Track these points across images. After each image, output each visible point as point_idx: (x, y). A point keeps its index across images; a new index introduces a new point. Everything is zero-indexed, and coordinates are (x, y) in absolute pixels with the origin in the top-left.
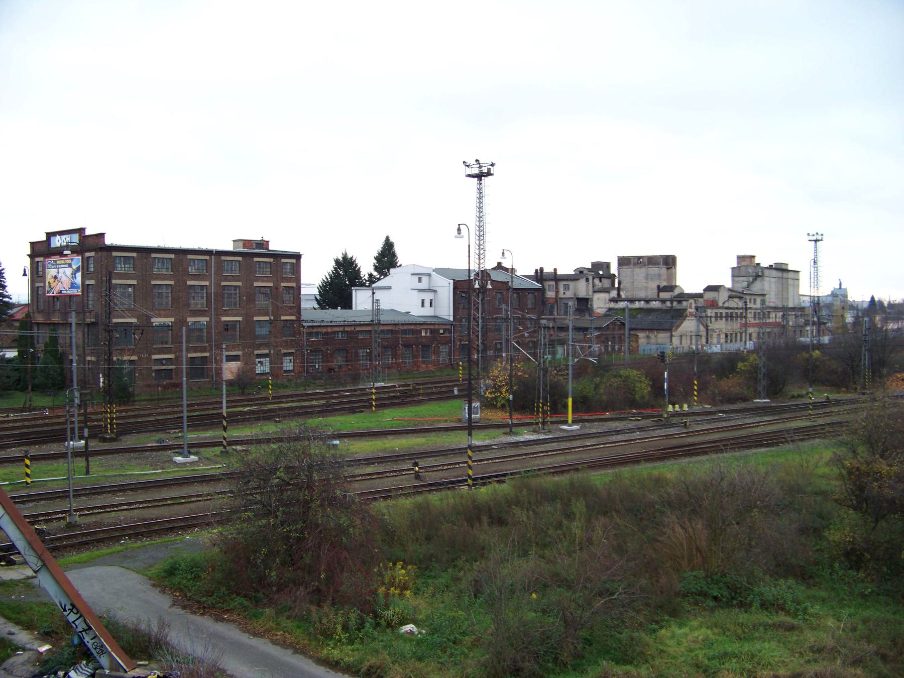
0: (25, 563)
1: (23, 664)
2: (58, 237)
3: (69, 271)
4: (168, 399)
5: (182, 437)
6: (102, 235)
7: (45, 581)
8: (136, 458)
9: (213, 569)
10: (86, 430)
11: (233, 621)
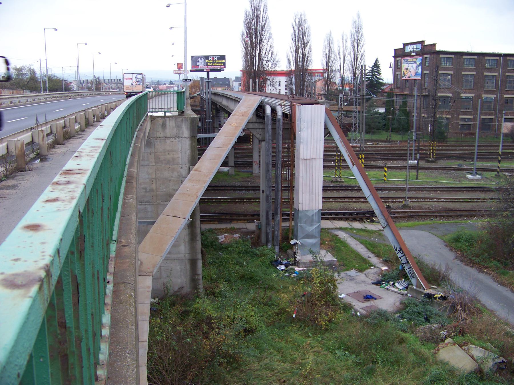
0: (379, 222)
1: (374, 274)
2: (409, 46)
3: (414, 65)
4: (467, 141)
5: (473, 164)
6: (434, 45)
7: (388, 233)
8: (445, 173)
9: (481, 242)
10: (418, 155)
11: (489, 274)
